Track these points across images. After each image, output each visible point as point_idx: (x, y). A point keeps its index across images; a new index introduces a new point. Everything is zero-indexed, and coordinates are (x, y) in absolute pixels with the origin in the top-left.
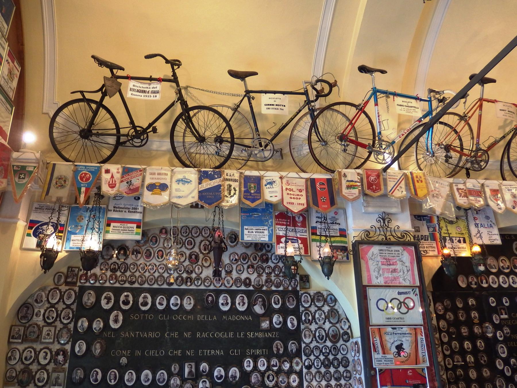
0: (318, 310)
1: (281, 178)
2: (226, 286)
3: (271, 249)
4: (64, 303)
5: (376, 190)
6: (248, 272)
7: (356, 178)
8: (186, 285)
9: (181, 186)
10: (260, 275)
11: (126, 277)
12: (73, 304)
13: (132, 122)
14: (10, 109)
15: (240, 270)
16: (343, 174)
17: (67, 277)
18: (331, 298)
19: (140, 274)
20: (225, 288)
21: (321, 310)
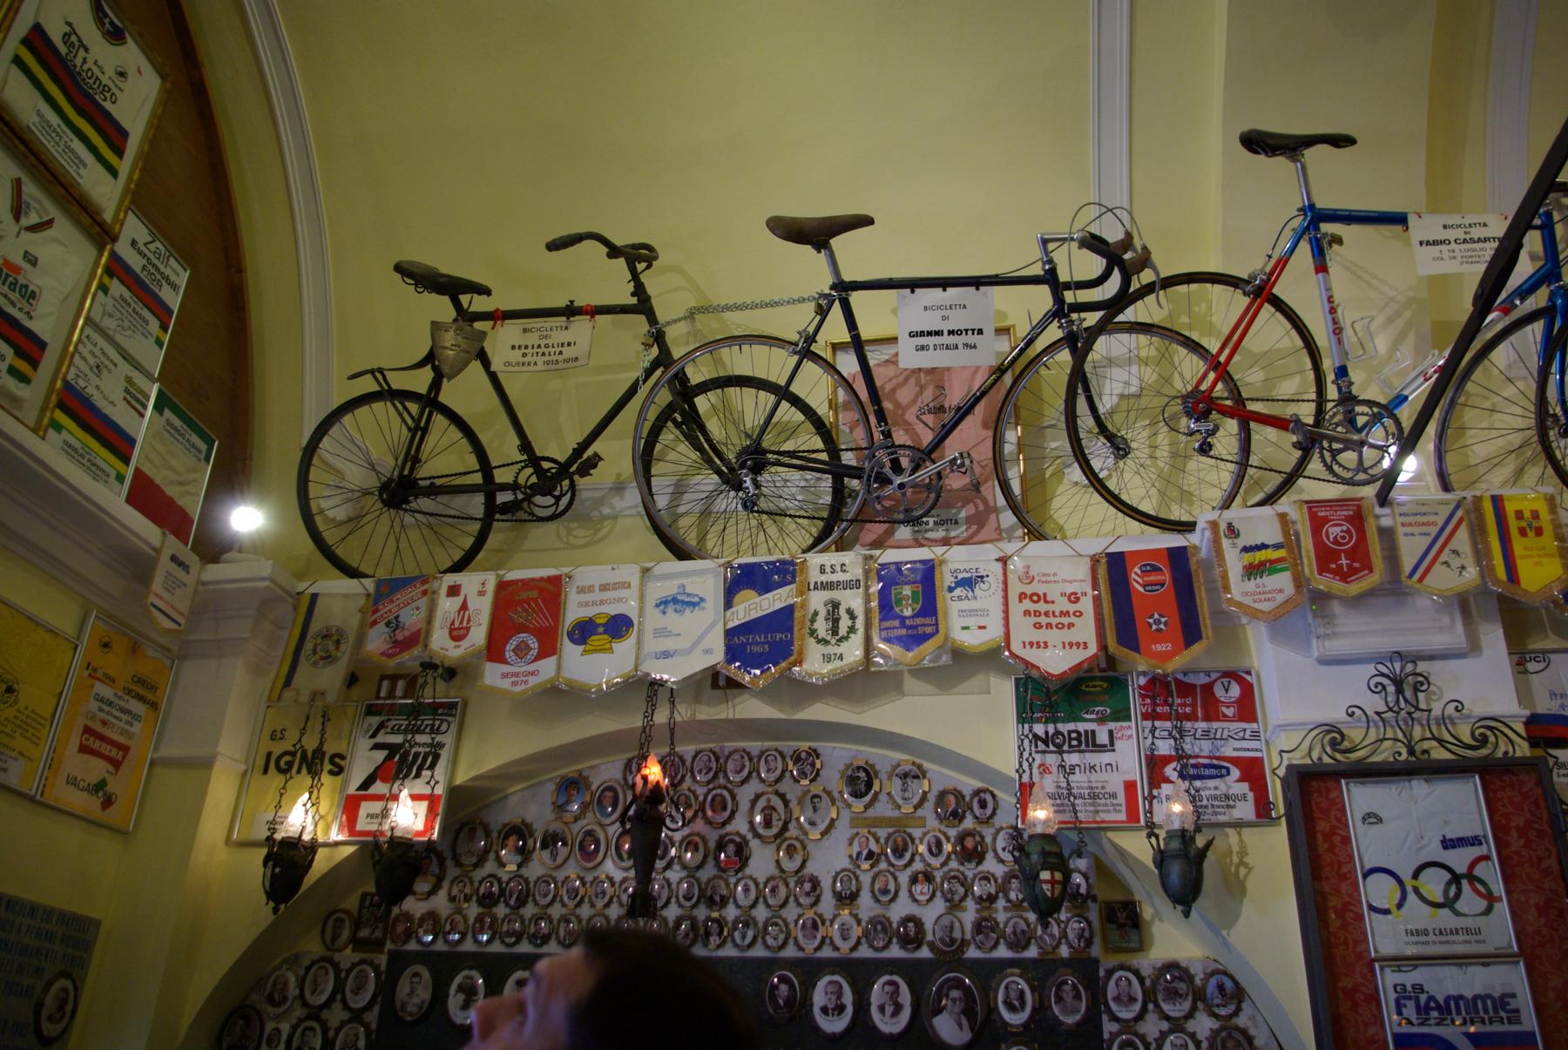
0: (1171, 1031)
1: (1004, 561)
2: (836, 949)
3: (994, 813)
4: (346, 1007)
5: (1353, 571)
6: (911, 895)
7: (1273, 535)
8: (706, 945)
9: (672, 619)
10: (954, 906)
11: (523, 922)
12: (369, 1007)
13: (526, 446)
14: (203, 447)
15: (885, 891)
16: (1223, 527)
17: (357, 924)
18: (1221, 987)
19: (564, 911)
20: (835, 955)
21: (1183, 1030)
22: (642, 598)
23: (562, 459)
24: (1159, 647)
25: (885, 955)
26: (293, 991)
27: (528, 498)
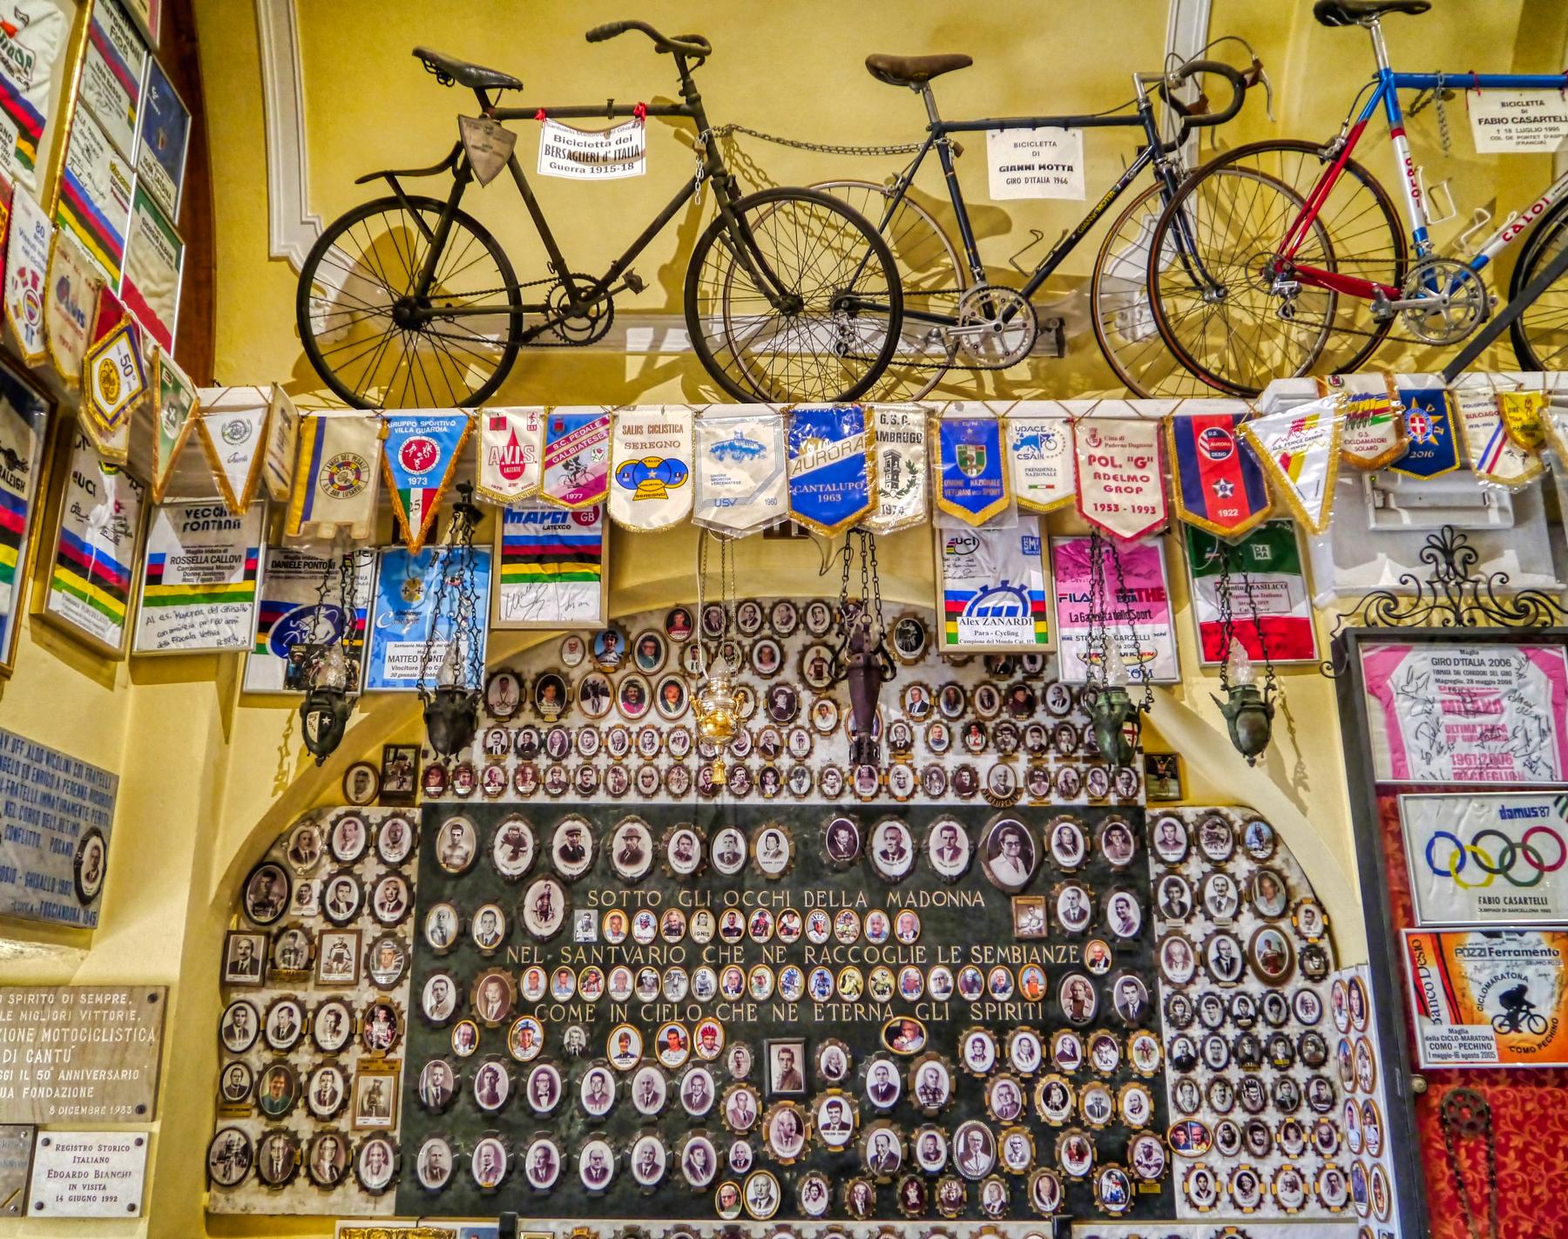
2: (893, 796)
6: (965, 746)
8: (762, 794)
13: (558, 263)
15: (939, 742)
17: (382, 779)
18: (1258, 833)
20: (893, 802)
22: (696, 439)
23: (599, 278)
24: (1225, 513)
25: (941, 802)
26: (320, 846)
27: (561, 321)
